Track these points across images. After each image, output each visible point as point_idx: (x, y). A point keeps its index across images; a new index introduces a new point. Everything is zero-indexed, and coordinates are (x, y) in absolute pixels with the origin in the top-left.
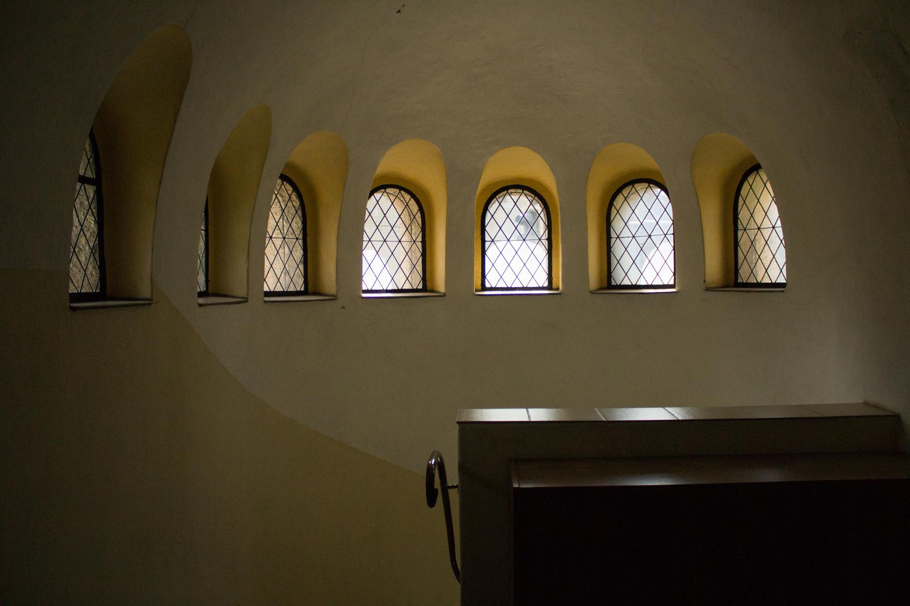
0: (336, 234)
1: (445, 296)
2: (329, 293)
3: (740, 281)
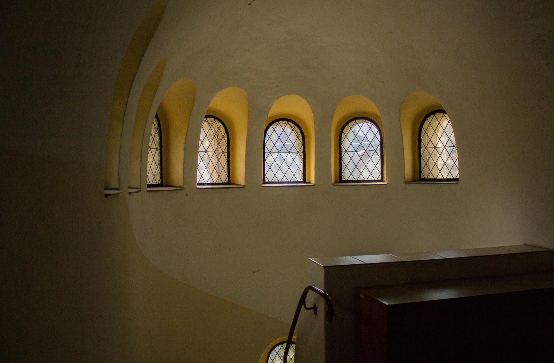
0: (184, 146)
1: (245, 187)
2: (177, 186)
3: (422, 177)
